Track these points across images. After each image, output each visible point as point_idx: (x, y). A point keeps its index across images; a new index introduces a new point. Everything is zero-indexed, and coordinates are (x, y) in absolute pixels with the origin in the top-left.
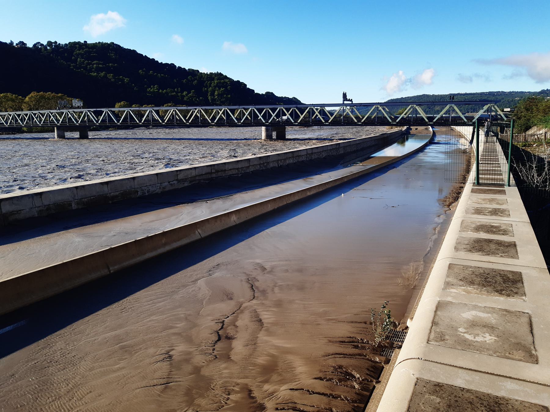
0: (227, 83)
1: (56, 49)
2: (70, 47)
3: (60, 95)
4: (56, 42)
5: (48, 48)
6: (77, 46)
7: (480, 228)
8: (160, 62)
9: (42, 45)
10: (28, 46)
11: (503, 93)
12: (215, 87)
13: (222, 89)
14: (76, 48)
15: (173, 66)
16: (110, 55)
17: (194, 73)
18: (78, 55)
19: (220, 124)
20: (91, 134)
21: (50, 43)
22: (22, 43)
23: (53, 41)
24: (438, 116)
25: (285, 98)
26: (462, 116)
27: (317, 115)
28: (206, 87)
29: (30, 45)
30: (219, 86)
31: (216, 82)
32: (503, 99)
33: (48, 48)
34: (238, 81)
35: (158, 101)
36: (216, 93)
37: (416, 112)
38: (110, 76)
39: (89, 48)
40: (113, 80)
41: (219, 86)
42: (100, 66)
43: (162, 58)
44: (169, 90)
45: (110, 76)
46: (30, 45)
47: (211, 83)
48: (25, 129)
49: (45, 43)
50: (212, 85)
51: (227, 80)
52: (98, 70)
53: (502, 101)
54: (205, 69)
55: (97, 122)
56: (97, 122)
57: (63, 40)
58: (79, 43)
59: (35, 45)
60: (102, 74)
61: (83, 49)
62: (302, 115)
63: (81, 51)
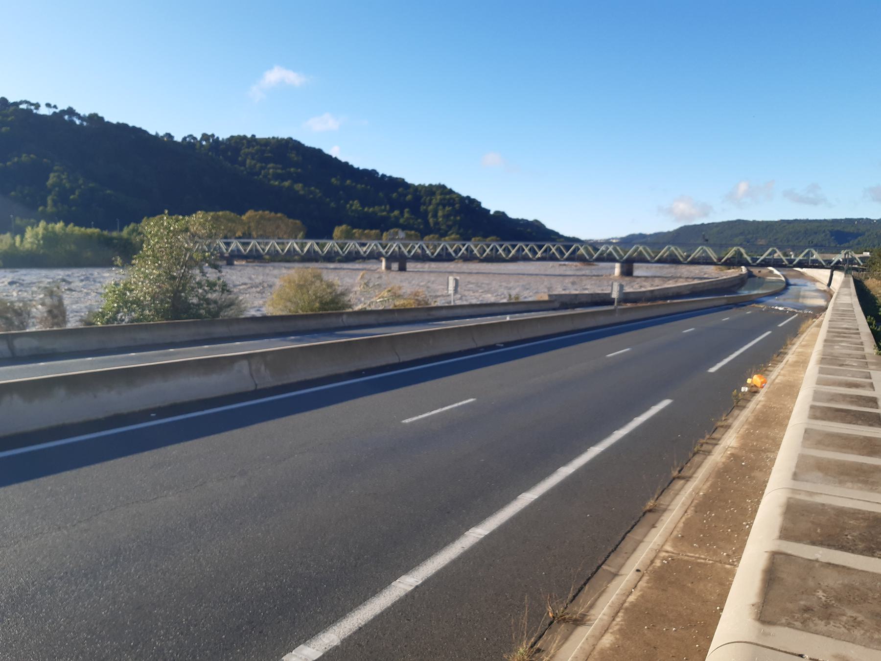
0: (454, 200)
1: (214, 145)
2: (236, 142)
3: (279, 215)
4: (213, 135)
5: (204, 143)
6: (245, 141)
7: (833, 398)
8: (361, 168)
9: (195, 138)
10: (175, 139)
11: (869, 221)
12: (438, 205)
13: (447, 209)
14: (243, 144)
15: (374, 172)
16: (288, 153)
17: (397, 184)
18: (247, 155)
19: (489, 260)
20: (410, 266)
21: (205, 137)
22: (169, 136)
23: (210, 133)
24: (762, 258)
25: (523, 220)
26: (784, 258)
27: (476, 247)
28: (424, 204)
29: (178, 138)
30: (443, 204)
31: (439, 197)
32: (868, 230)
33: (204, 143)
34: (346, 163)
35: (381, 225)
36: (440, 213)
37: (705, 251)
38: (298, 187)
39: (261, 145)
40: (302, 192)
41: (443, 204)
42: (279, 171)
43: (360, 162)
44: (377, 208)
45: (298, 187)
46: (178, 138)
47: (431, 200)
48: (267, 257)
49: (199, 137)
50: (434, 201)
51: (454, 196)
52: (277, 177)
53: (867, 234)
54: (415, 178)
55: (283, 250)
56: (283, 250)
57: (223, 134)
58: (245, 137)
59: (185, 139)
60: (287, 184)
61: (253, 146)
62: (567, 251)
63: (250, 150)
